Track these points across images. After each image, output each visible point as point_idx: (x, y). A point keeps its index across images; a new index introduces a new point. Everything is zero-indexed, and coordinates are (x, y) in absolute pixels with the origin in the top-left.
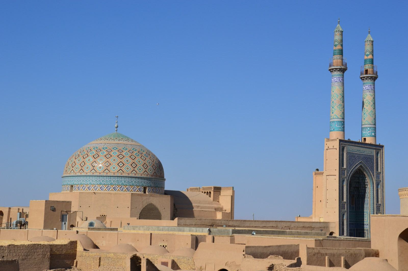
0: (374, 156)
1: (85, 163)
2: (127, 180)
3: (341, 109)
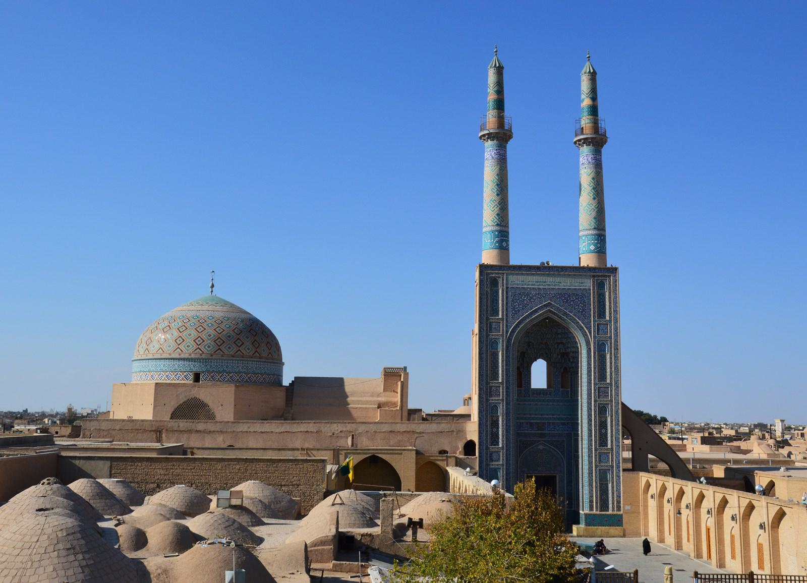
0: (590, 289)
1: (176, 342)
2: (167, 362)
3: (495, 208)
